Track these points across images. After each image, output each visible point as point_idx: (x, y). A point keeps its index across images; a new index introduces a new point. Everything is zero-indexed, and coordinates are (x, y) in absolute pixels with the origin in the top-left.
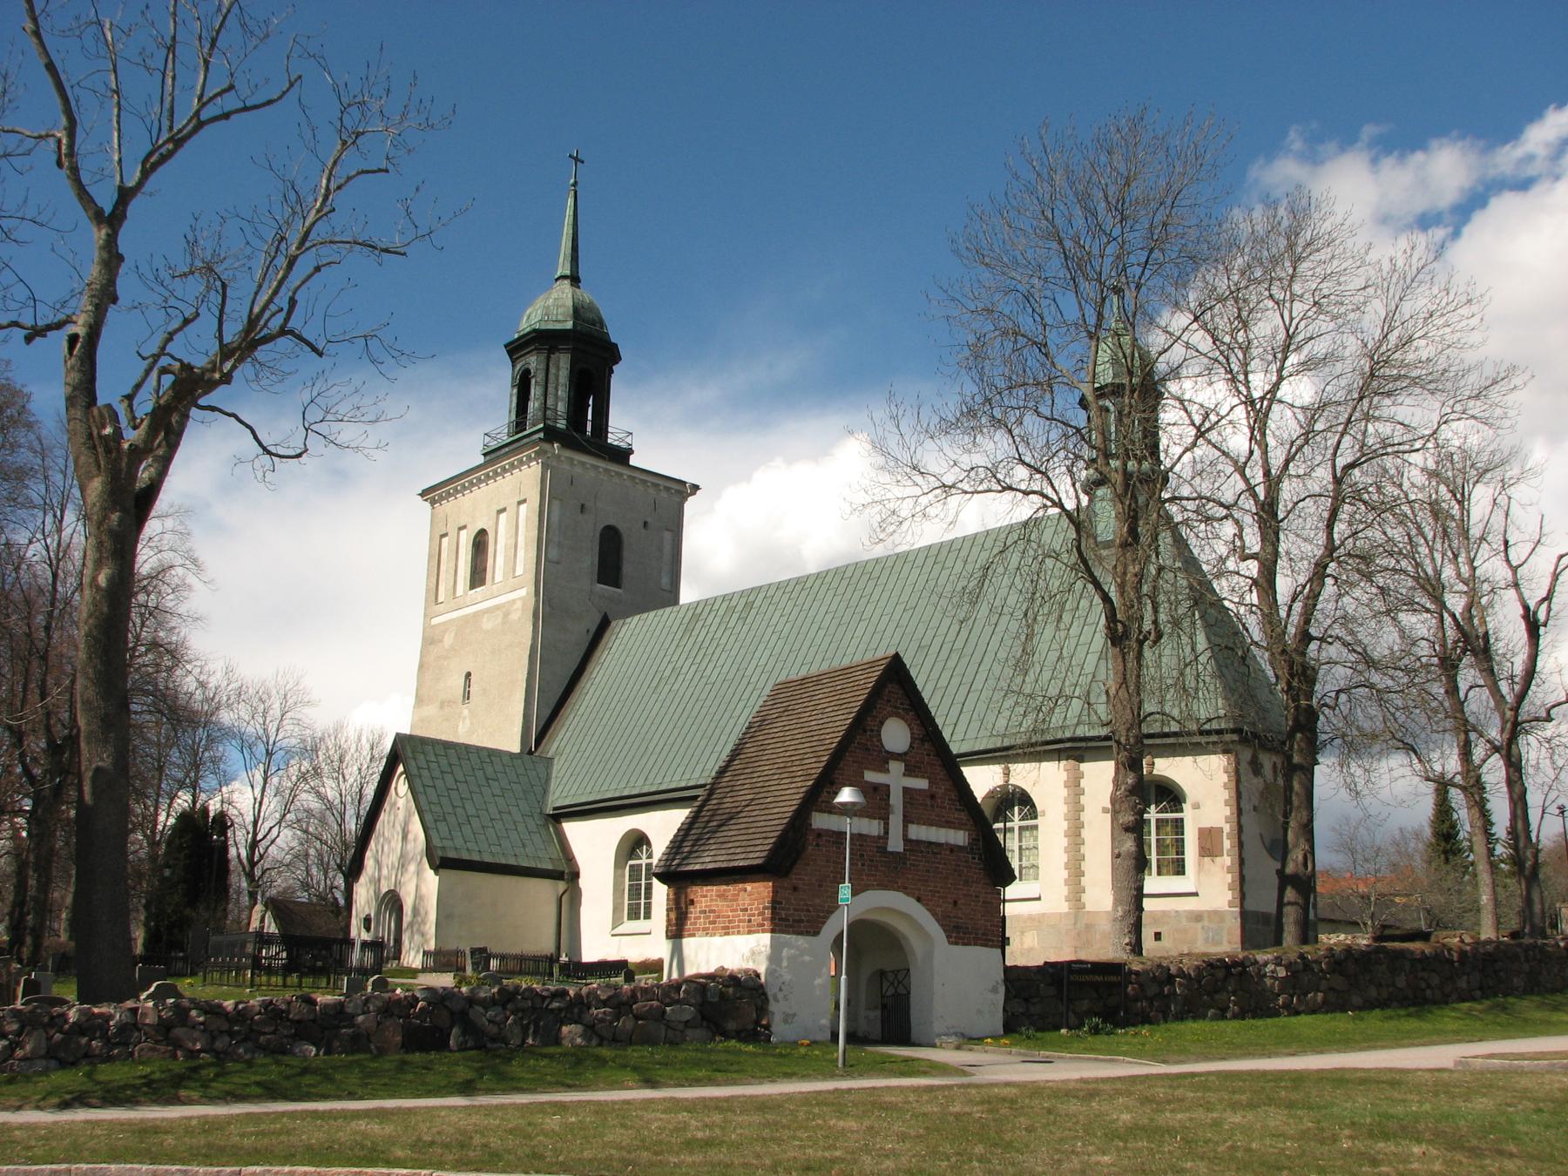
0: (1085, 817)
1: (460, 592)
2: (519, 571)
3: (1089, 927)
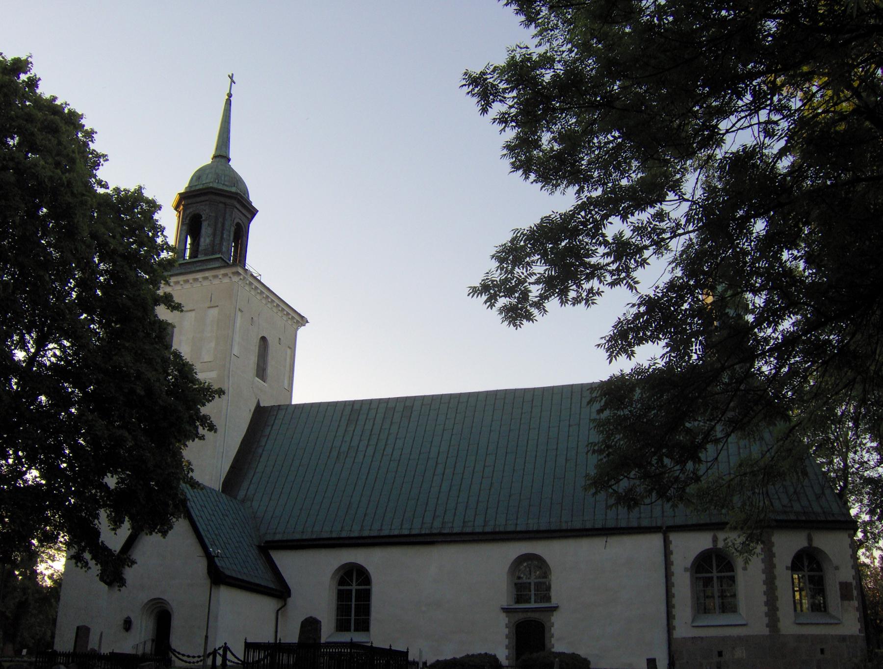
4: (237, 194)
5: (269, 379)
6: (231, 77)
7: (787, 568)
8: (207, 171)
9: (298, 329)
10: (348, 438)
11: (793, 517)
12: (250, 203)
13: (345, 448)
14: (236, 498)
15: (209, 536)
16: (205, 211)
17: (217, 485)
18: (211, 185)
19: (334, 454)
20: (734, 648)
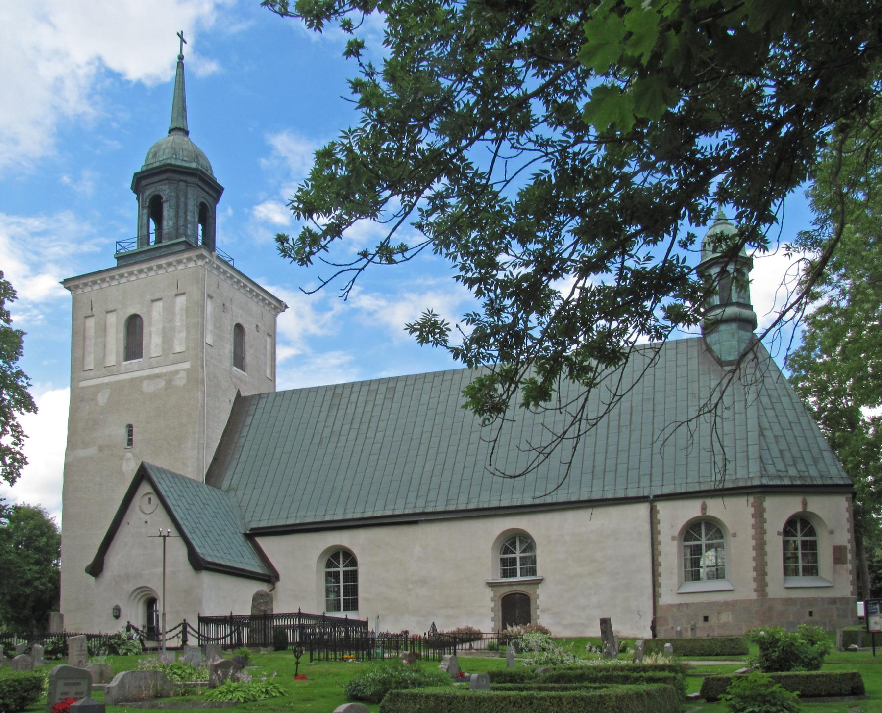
0: (767, 537)
1: (111, 360)
4: (197, 169)
6: (181, 36)
8: (163, 147)
9: (276, 315)
10: (330, 423)
11: (787, 482)
14: (220, 488)
15: (187, 524)
16: (165, 191)
17: (202, 478)
18: (168, 161)
19: (316, 440)
20: (719, 613)
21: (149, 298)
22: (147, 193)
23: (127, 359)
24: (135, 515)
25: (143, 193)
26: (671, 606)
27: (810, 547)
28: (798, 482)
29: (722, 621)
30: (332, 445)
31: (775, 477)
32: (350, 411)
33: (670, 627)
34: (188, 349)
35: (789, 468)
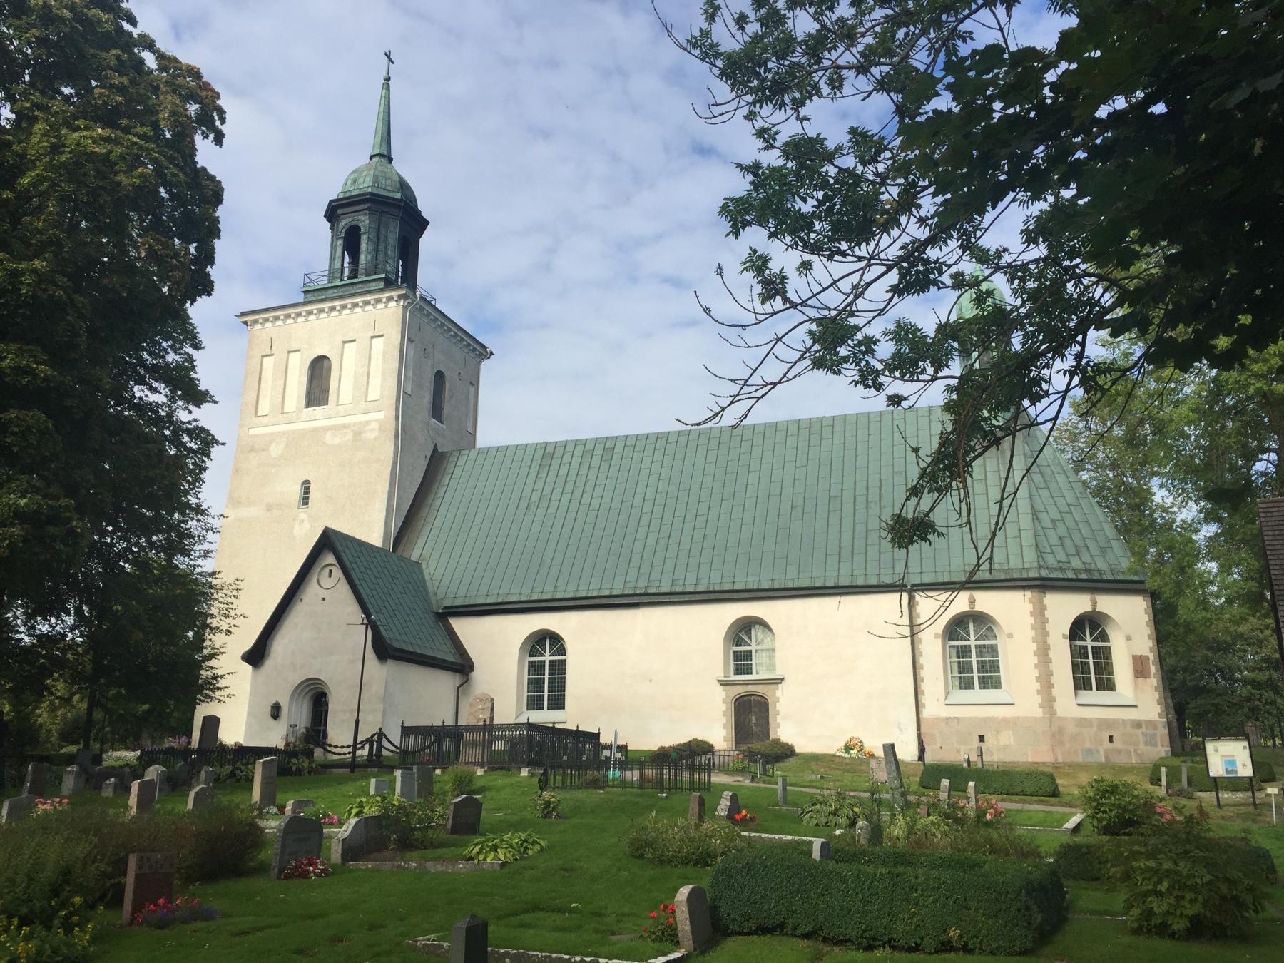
0: (1051, 640)
2: (374, 394)
3: (1061, 730)
5: (444, 418)
7: (1064, 636)
10: (539, 486)
11: (1071, 575)
12: (419, 213)
13: (535, 497)
15: (373, 601)
16: (364, 221)
19: (524, 504)
21: (340, 339)
22: (343, 223)
23: (308, 405)
24: (312, 591)
25: (339, 222)
26: (938, 719)
27: (1103, 655)
28: (1084, 576)
29: (1002, 743)
30: (541, 512)
31: (1056, 569)
32: (563, 471)
33: (938, 745)
34: (382, 397)
35: (1072, 559)
